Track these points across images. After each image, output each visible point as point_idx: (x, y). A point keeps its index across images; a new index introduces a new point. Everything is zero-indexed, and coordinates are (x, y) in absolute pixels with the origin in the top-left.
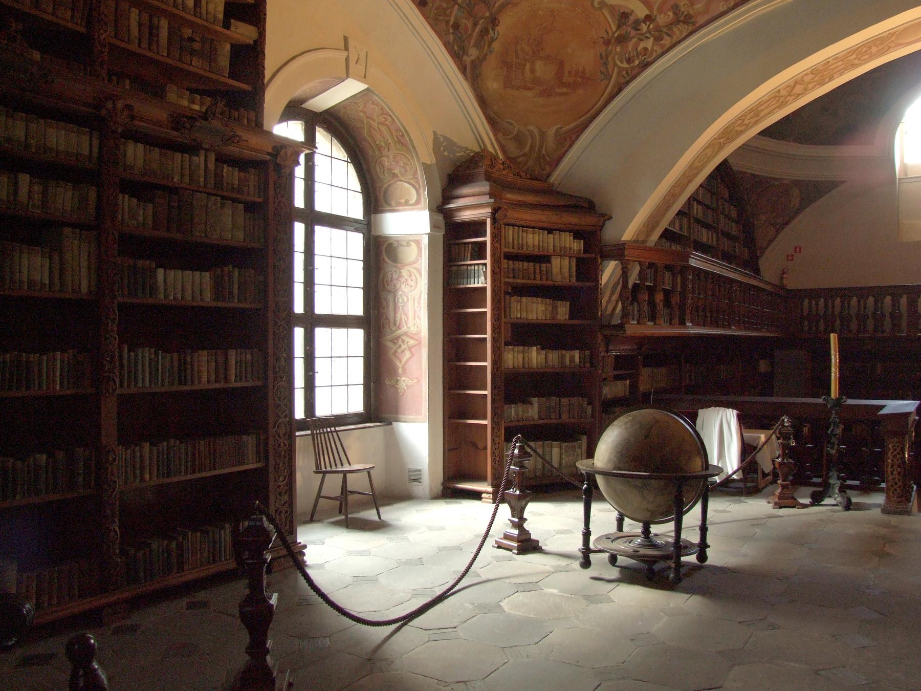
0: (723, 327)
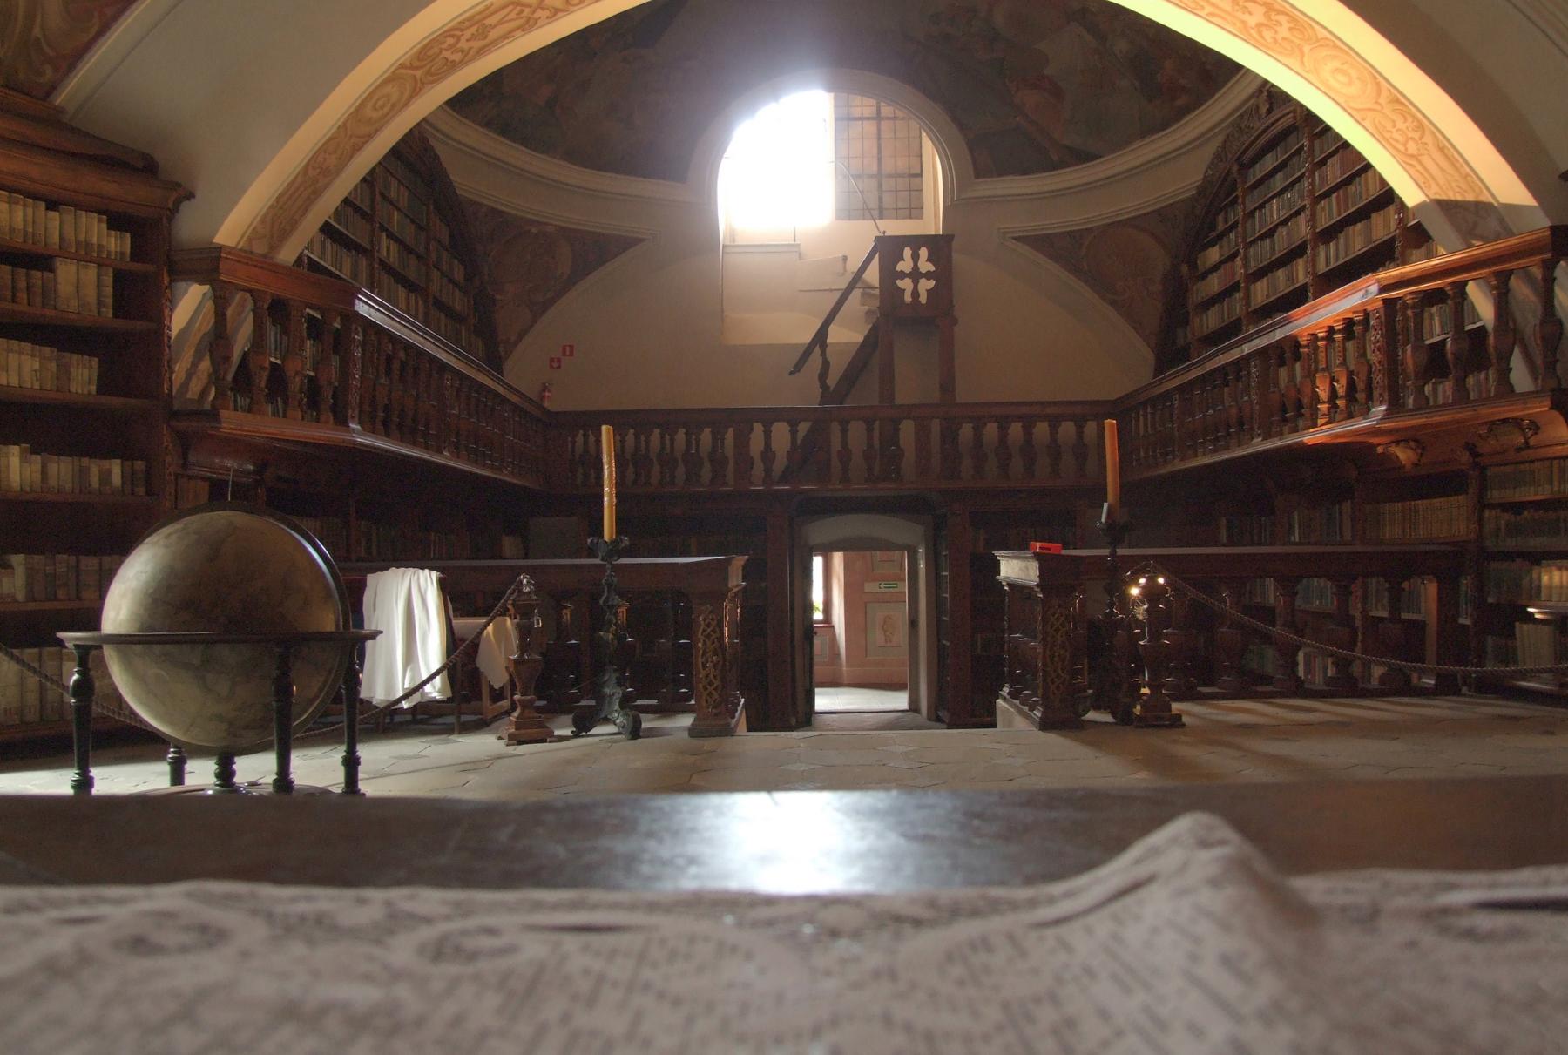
0: (427, 448)
